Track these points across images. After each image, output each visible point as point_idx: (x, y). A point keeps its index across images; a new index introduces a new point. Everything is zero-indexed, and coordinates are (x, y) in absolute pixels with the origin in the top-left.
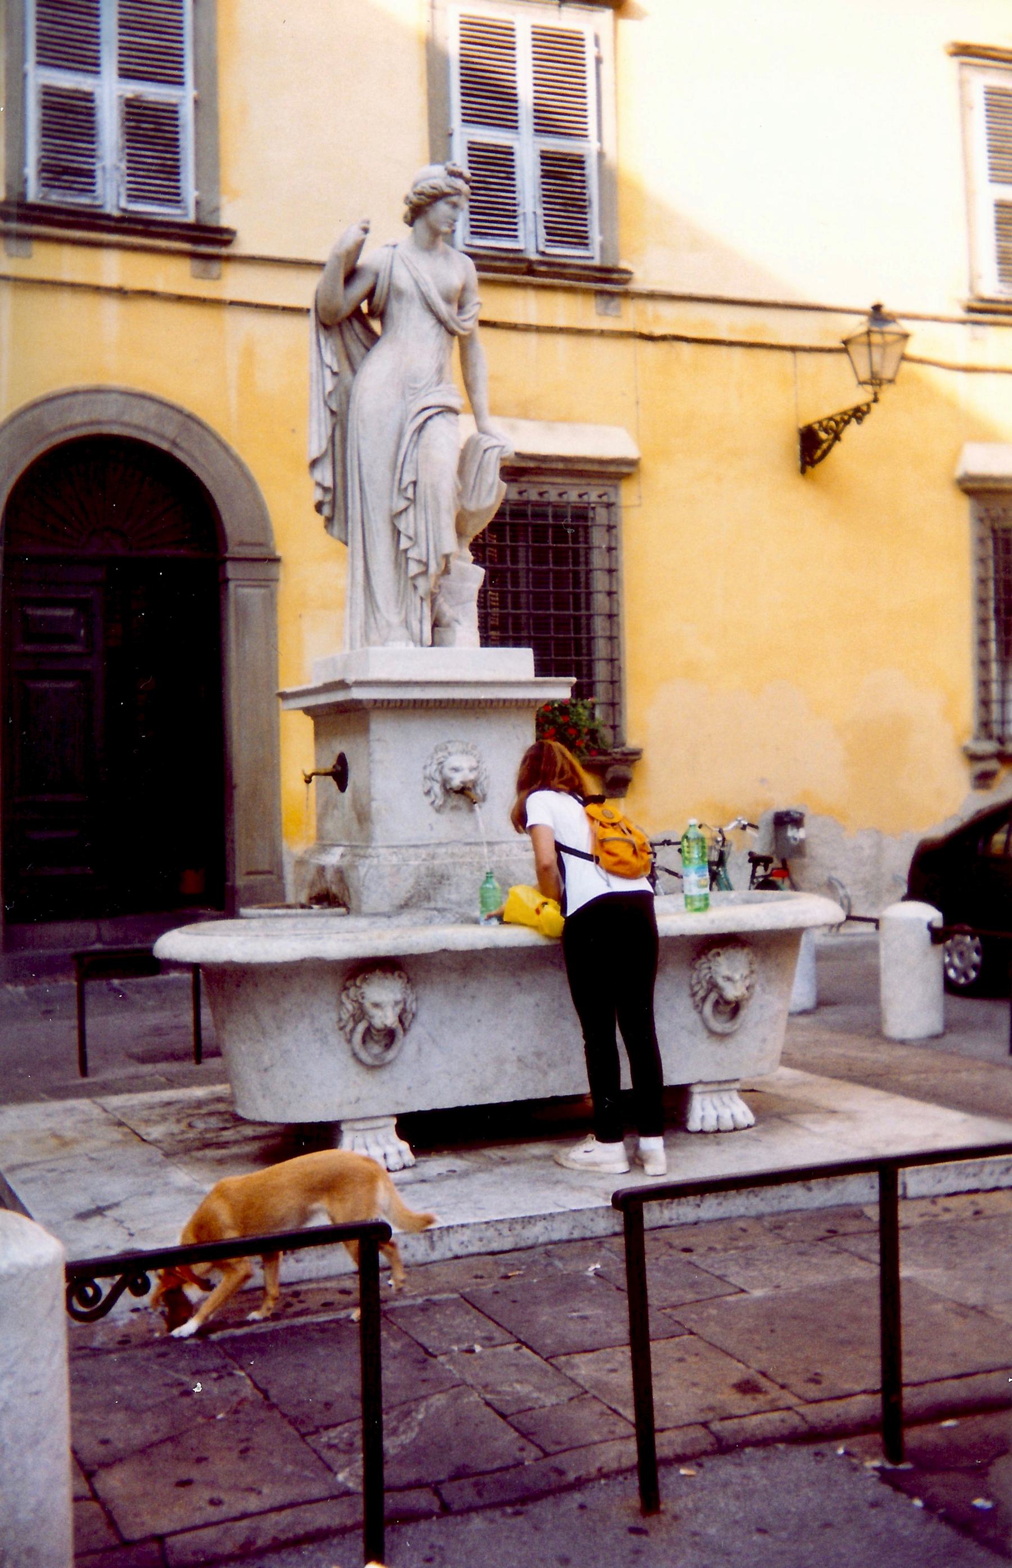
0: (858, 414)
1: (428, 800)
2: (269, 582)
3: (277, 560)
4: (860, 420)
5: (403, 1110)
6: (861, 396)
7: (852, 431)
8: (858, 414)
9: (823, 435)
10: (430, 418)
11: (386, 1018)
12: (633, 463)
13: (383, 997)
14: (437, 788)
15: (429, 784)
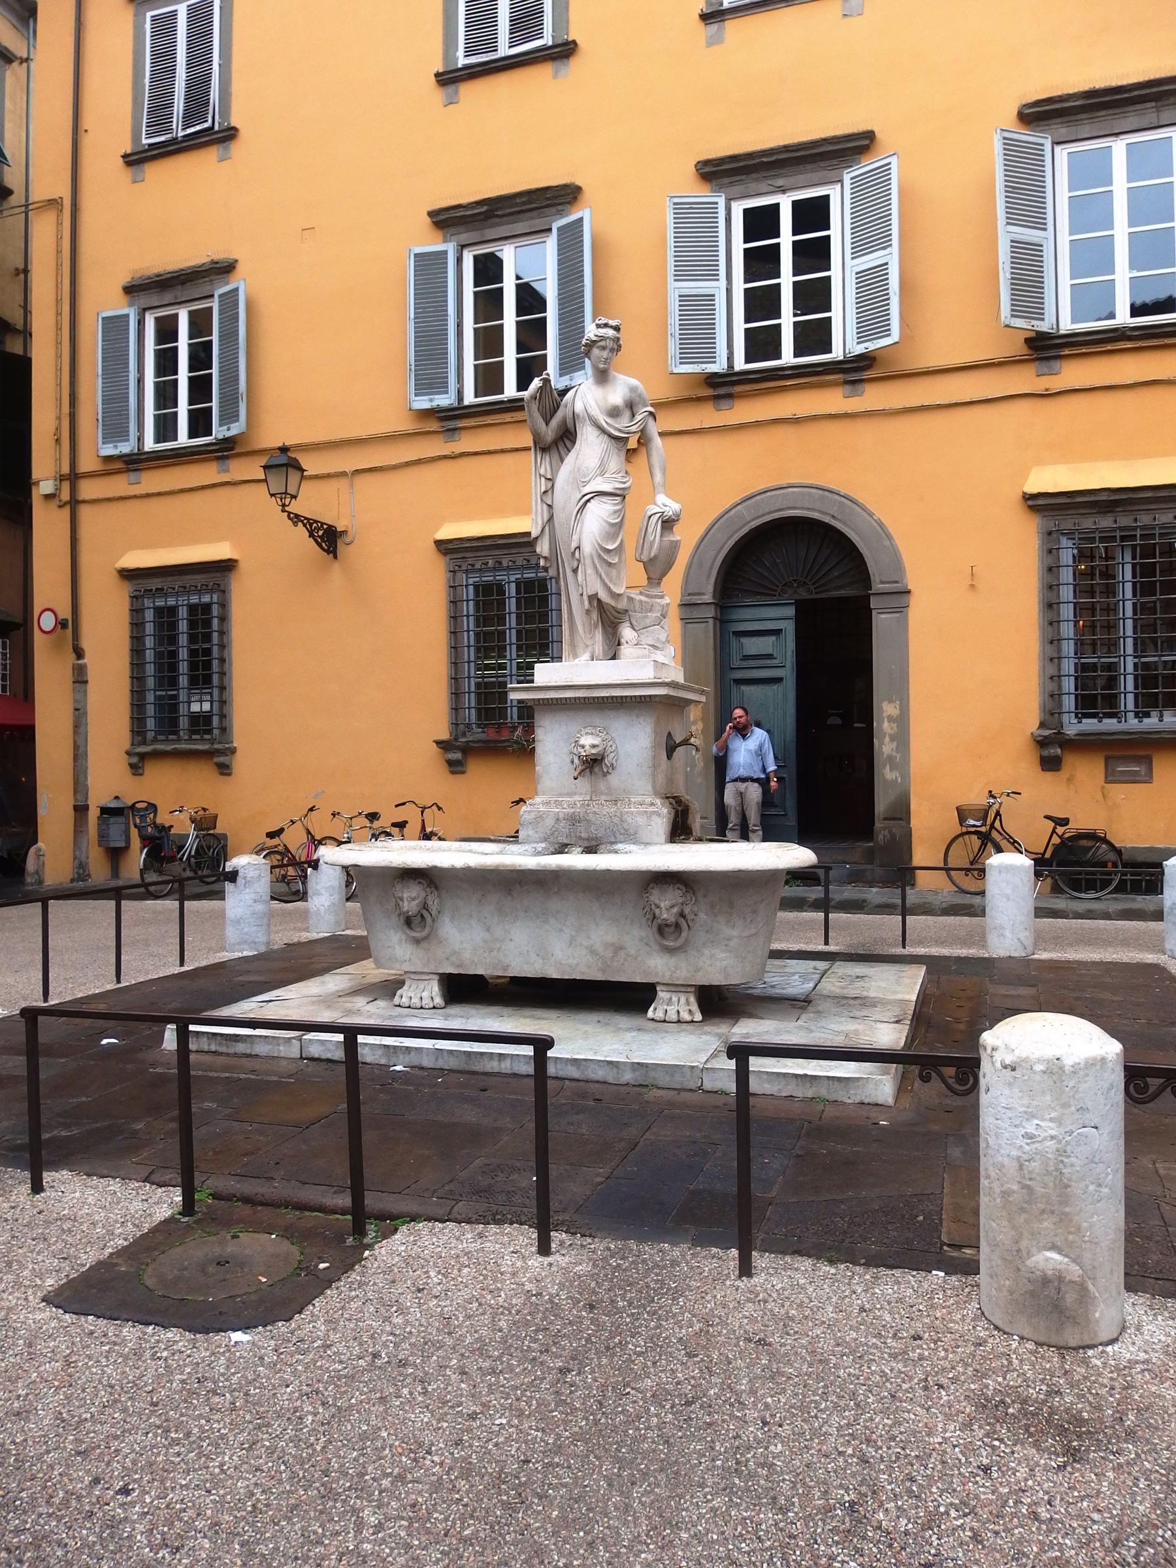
2: (902, 609)
3: (909, 592)
10: (588, 501)
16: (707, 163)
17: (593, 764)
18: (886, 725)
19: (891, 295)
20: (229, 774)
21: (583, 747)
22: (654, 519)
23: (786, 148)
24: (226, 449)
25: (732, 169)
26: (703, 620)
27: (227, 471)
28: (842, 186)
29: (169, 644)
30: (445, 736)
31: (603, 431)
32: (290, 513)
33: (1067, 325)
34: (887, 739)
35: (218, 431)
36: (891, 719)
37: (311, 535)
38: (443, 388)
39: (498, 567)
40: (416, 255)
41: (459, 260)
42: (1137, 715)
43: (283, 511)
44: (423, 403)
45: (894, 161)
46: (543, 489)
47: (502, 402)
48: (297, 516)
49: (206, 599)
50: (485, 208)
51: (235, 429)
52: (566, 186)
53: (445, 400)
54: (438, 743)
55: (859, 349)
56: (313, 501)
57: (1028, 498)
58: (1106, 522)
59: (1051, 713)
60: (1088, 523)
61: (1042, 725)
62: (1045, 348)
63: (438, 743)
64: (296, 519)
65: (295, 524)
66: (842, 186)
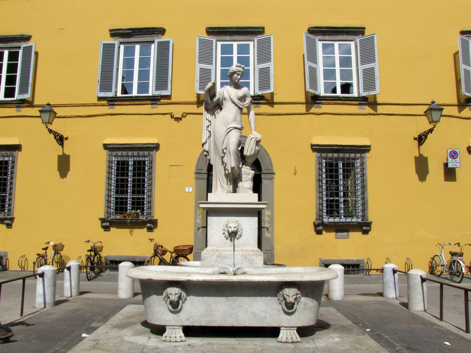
0: (431, 131)
1: (224, 236)
2: (272, 179)
3: (274, 174)
4: (431, 132)
5: (298, 325)
6: (431, 126)
7: (430, 136)
8: (431, 131)
9: (423, 137)
10: (231, 130)
11: (291, 299)
12: (369, 146)
13: (290, 293)
14: (227, 233)
15: (224, 231)
16: (210, 28)
17: (233, 235)
18: (266, 218)
19: (271, 77)
20: (11, 228)
21: (231, 228)
22: (253, 140)
23: (237, 28)
24: (22, 103)
25: (218, 32)
26: (203, 179)
27: (20, 111)
28: (254, 42)
29: (4, 175)
30: (103, 216)
31: (236, 105)
32: (49, 129)
33: (322, 94)
34: (267, 223)
35: (17, 96)
36: (268, 216)
37: (55, 138)
38: (110, 90)
39: (128, 156)
40: (104, 44)
41: (119, 47)
42: (344, 217)
43: (47, 128)
44: (103, 95)
45: (272, 36)
46: (207, 125)
47: (132, 97)
48: (51, 130)
49: (6, 159)
50: (131, 31)
51: (27, 96)
52: (161, 28)
53: (110, 94)
54: (100, 219)
55: (260, 93)
56: (57, 125)
57: (312, 146)
58: (336, 155)
59: (320, 217)
60: (330, 155)
61: (317, 219)
62: (313, 100)
63: (100, 219)
64: (50, 131)
65: (50, 133)
66: (254, 42)
